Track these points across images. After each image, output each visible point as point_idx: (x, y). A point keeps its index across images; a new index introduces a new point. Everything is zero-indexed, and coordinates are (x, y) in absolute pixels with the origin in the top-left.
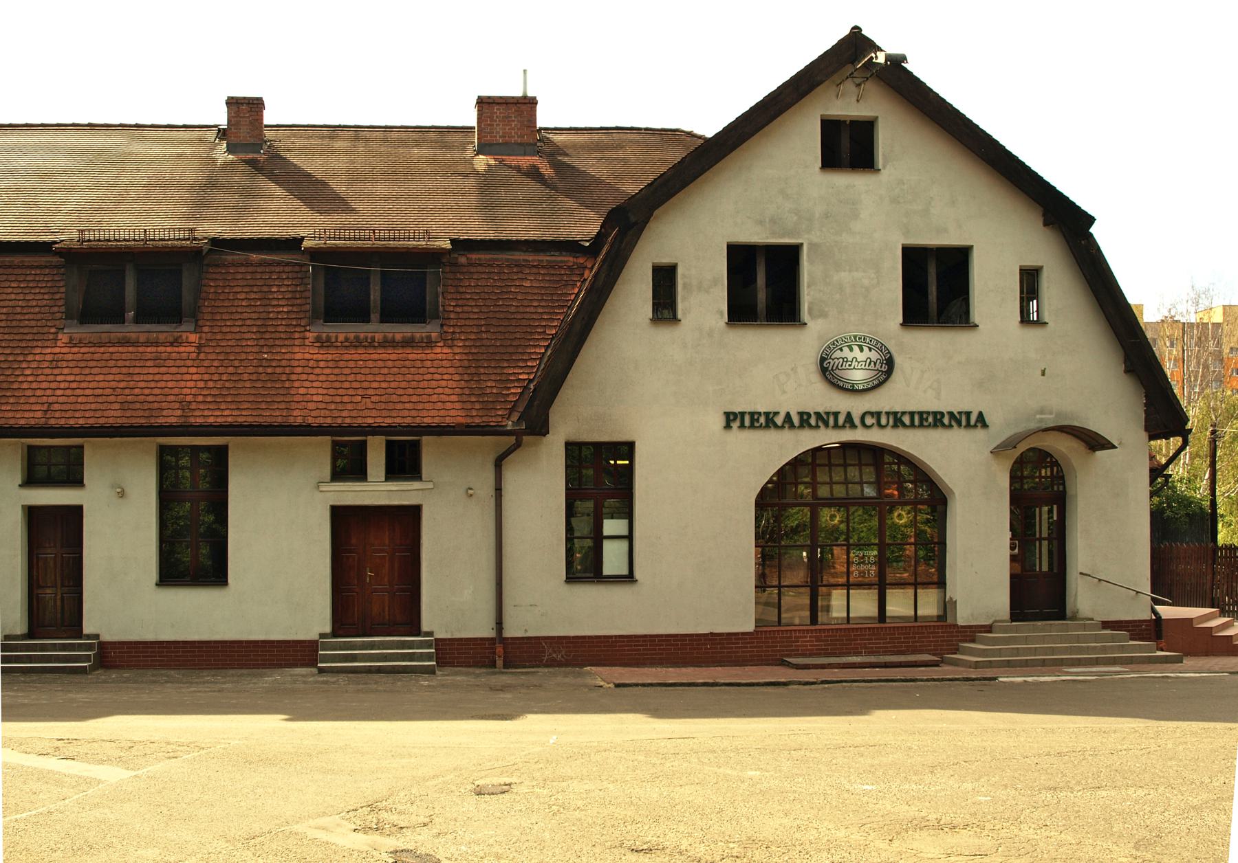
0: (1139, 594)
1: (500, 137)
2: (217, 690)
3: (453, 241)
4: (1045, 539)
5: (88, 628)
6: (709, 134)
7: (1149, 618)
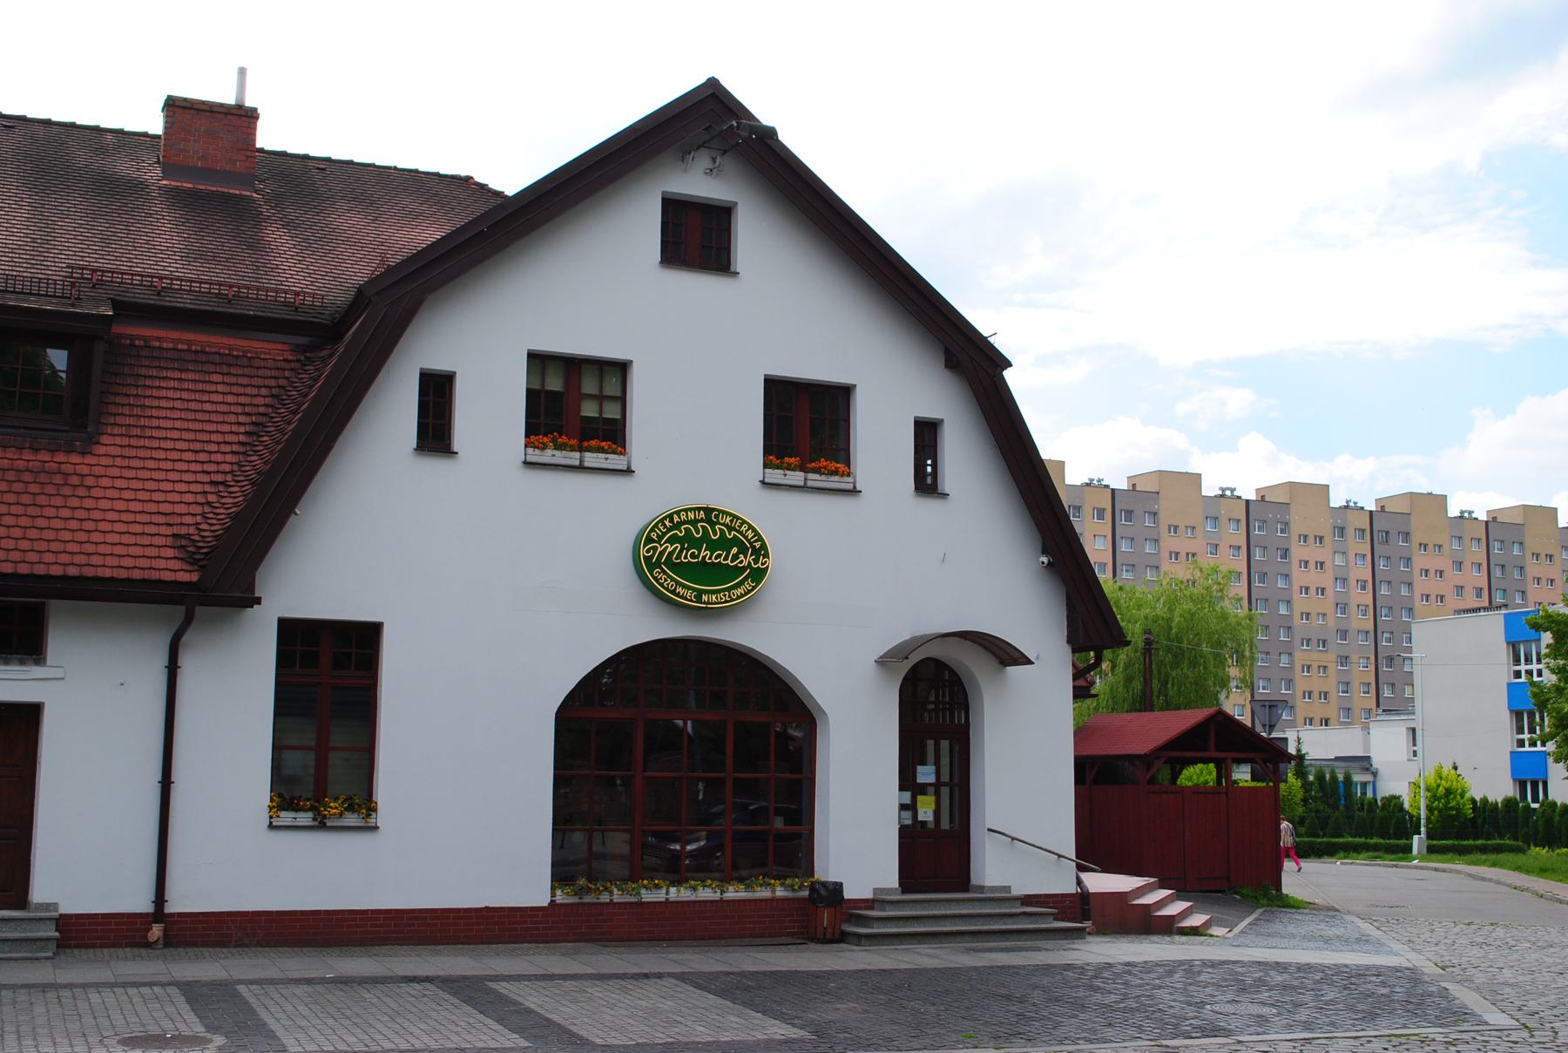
0: (1062, 859)
1: (198, 159)
2: (1215, 938)
3: (116, 304)
4: (945, 784)
5: (40, 891)
6: (511, 190)
7: (1075, 892)
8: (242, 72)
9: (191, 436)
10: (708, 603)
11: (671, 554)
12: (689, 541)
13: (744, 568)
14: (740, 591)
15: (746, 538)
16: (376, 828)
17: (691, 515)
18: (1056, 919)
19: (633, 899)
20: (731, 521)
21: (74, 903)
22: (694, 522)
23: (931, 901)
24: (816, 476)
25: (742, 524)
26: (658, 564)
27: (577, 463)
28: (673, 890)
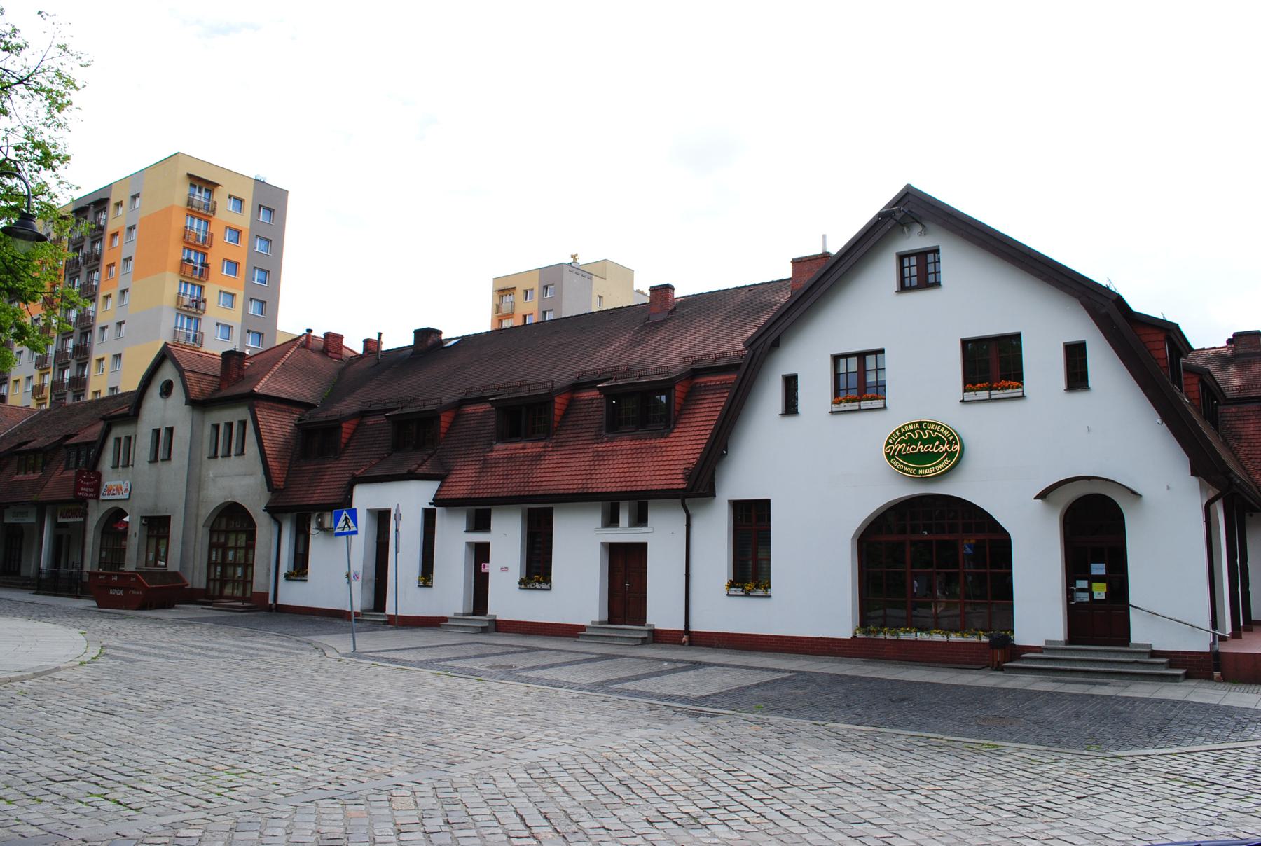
8: (824, 236)
9: (705, 423)
10: (923, 474)
11: (900, 450)
12: (911, 441)
13: (943, 453)
14: (941, 466)
15: (944, 435)
16: (770, 596)
17: (911, 427)
18: (1167, 669)
19: (895, 638)
20: (934, 427)
21: (501, 617)
22: (913, 431)
23: (1082, 650)
24: (996, 392)
25: (896, 434)
26: (893, 456)
27: (857, 408)
28: (918, 634)
